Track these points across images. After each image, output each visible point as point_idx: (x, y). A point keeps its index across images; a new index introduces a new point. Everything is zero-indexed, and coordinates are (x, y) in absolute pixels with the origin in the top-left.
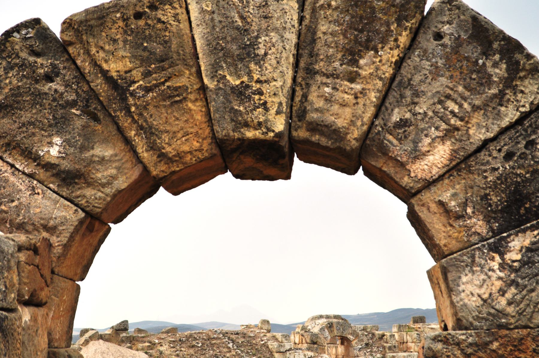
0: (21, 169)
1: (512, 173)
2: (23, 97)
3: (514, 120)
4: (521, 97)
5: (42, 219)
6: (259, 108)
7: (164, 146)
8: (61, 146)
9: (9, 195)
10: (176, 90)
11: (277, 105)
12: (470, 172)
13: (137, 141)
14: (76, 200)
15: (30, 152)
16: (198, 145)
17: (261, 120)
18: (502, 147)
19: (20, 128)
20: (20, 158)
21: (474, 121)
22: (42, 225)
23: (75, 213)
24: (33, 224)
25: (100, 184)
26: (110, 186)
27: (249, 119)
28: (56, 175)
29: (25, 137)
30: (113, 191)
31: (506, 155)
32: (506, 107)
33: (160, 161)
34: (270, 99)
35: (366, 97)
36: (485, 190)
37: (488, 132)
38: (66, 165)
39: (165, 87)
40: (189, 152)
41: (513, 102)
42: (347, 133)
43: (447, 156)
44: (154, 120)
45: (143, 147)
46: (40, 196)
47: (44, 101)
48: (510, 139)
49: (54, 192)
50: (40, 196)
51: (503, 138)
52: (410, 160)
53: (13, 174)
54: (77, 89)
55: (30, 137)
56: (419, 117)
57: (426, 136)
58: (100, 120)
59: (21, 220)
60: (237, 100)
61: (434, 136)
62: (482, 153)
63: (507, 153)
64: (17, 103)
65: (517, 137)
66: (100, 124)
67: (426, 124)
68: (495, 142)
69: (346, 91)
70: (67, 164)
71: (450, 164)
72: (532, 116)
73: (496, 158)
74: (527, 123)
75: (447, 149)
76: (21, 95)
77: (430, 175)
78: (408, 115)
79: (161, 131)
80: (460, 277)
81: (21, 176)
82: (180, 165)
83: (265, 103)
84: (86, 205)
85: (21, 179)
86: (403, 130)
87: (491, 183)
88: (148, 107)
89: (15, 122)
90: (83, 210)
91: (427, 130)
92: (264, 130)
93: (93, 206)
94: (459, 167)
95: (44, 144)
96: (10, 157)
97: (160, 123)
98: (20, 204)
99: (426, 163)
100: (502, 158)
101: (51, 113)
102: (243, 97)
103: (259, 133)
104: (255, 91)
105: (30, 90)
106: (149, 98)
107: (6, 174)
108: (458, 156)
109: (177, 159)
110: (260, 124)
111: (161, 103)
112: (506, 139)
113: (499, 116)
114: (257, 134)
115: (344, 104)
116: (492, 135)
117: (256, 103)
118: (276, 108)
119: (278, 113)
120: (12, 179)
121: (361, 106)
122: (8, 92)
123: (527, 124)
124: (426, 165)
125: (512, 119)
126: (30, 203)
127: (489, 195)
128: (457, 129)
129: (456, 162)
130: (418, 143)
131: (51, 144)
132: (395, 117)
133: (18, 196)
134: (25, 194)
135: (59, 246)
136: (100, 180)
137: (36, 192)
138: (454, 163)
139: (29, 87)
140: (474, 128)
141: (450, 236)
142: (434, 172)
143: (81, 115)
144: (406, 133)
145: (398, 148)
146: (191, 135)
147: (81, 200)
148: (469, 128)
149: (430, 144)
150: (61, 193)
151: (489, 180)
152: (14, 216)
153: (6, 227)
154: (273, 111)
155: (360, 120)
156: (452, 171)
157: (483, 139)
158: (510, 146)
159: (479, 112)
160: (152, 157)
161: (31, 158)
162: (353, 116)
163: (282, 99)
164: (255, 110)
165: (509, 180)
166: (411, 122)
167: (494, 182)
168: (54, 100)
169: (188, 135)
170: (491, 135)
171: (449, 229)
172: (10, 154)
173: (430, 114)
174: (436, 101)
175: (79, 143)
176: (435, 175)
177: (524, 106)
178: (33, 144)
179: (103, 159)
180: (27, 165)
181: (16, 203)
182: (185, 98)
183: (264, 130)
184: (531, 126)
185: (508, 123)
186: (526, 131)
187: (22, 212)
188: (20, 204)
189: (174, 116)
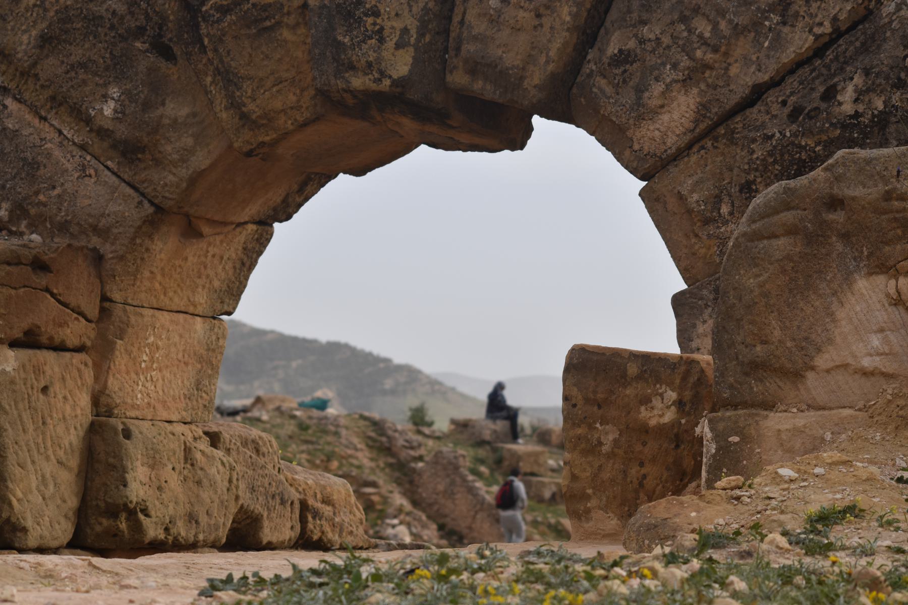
0: (69, 136)
1: (793, 143)
2: (72, 24)
3: (804, 49)
4: (819, 8)
5: (90, 215)
6: (372, 38)
7: (245, 101)
8: (119, 100)
9: (50, 178)
10: (265, 10)
11: (398, 33)
12: (732, 142)
13: (214, 92)
14: (141, 187)
15: (79, 111)
16: (294, 98)
17: (371, 59)
18: (789, 97)
19: (67, 72)
20: (68, 119)
21: (738, 52)
22: (91, 226)
23: (137, 207)
24: (78, 224)
25: (170, 161)
26: (185, 165)
27: (354, 56)
28: (114, 146)
29: (72, 86)
30: (190, 172)
31: (792, 111)
32: (793, 26)
33: (243, 126)
34: (389, 24)
35: (555, 15)
36: (748, 174)
37: (759, 71)
38: (122, 131)
39: (250, 5)
40: (283, 110)
41: (804, 17)
42: (522, 78)
43: (690, 115)
44: (232, 60)
45: (221, 103)
46: (93, 180)
47: (99, 29)
48: (801, 83)
49: (114, 173)
50: (93, 180)
51: (790, 81)
52: (631, 121)
53: (61, 145)
54: (147, 9)
55: (80, 86)
56: (649, 47)
57: (657, 79)
58: (175, 59)
59: (62, 217)
60: (343, 26)
61: (668, 80)
62: (755, 110)
63: (794, 107)
64: (66, 32)
65: (813, 79)
66: (175, 64)
67: (659, 58)
68: (778, 89)
69: (522, 4)
70: (124, 129)
71: (695, 128)
72: (841, 42)
73: (775, 116)
74: (830, 55)
75: (692, 101)
76: (70, 19)
77: (663, 148)
78: (632, 44)
79: (241, 77)
80: (694, 326)
81: (70, 148)
82: (270, 133)
83: (382, 29)
84: (153, 194)
85: (71, 152)
86: (622, 69)
87: (758, 162)
88: (224, 39)
89: (63, 62)
90: (152, 203)
91: (658, 69)
92: (376, 75)
93: (163, 197)
94: (715, 134)
95: (98, 98)
96: (56, 119)
97: (240, 64)
98: (65, 191)
99: (658, 126)
100: (785, 118)
101: (108, 47)
102: (352, 21)
103: (370, 80)
104: (368, 10)
105: (82, 12)
106: (226, 24)
107: (49, 145)
108: (708, 115)
109: (264, 122)
110: (370, 65)
111: (243, 32)
112: (795, 83)
113: (778, 42)
114: (367, 81)
115: (518, 27)
116: (766, 77)
117: (367, 30)
118: (397, 38)
119: (398, 46)
120: (57, 153)
121: (546, 28)
122: (53, 17)
123: (831, 57)
124: (658, 129)
125: (801, 48)
126: (77, 192)
127: (754, 182)
128: (707, 67)
129: (705, 124)
130: (643, 92)
131: (105, 97)
132: (612, 49)
133: (62, 181)
134: (72, 175)
135: (113, 258)
136: (170, 155)
137: (87, 173)
138: (702, 126)
139: (81, 8)
140: (737, 65)
141: (694, 254)
142: (669, 142)
143: (147, 51)
144: (626, 75)
145: (611, 100)
146: (285, 84)
147: (148, 187)
148: (729, 64)
149: (663, 93)
150: (122, 175)
151: (755, 156)
152: (54, 212)
153: (47, 227)
154: (390, 44)
155: (544, 55)
156: (704, 141)
157: (750, 84)
158: (799, 95)
159: (746, 36)
160: (233, 118)
161: (82, 120)
162: (533, 48)
163: (408, 22)
164: (364, 41)
165: (786, 156)
166: (636, 56)
167: (763, 160)
168: (112, 27)
169: (281, 82)
170: (765, 77)
171: (693, 240)
172: (56, 113)
173: (666, 40)
174: (676, 17)
175: (142, 96)
176: (670, 148)
177: (821, 24)
178: (83, 98)
179: (175, 121)
180: (78, 131)
181: (58, 191)
182: (279, 24)
183: (376, 75)
184: (836, 58)
185: (793, 56)
186: (828, 67)
187: (65, 204)
188: (65, 191)
189: (262, 53)
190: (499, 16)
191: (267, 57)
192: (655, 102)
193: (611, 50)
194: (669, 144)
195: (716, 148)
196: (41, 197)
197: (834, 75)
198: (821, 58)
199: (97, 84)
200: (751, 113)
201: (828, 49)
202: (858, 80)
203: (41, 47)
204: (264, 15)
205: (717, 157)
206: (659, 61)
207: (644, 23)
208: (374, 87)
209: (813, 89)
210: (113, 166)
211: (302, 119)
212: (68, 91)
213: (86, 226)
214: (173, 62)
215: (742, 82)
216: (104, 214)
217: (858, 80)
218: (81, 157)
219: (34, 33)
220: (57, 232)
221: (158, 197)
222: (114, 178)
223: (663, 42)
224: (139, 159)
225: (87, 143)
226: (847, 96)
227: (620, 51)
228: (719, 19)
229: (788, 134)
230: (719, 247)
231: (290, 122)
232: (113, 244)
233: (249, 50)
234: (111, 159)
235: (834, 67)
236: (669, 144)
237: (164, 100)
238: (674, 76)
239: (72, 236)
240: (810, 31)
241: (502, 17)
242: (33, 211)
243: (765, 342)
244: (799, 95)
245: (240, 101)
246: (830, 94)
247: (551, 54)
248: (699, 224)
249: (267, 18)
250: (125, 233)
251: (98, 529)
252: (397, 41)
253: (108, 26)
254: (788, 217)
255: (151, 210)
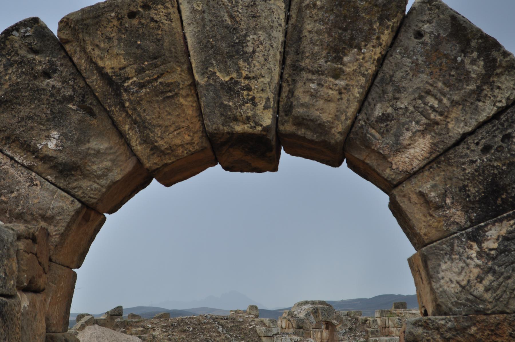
0: (20, 161)
1: (490, 165)
4: (498, 93)
5: (40, 209)
8: (58, 139)
9: (9, 186)
10: (168, 86)
11: (264, 100)
13: (131, 134)
14: (73, 192)
17: (249, 115)
18: (480, 140)
20: (19, 151)
21: (453, 115)
22: (40, 215)
23: (71, 204)
25: (95, 176)
26: (105, 178)
28: (54, 167)
29: (23, 131)
30: (108, 182)
32: (484, 102)
33: (153, 154)
34: (258, 95)
35: (350, 93)
37: (466, 126)
38: (63, 158)
39: (158, 83)
40: (181, 145)
41: (490, 98)
43: (427, 149)
44: (147, 115)
45: (137, 140)
47: (42, 96)
49: (52, 183)
50: (39, 188)
51: (481, 131)
53: (12, 166)
55: (29, 130)
57: (407, 130)
58: (95, 115)
59: (20, 210)
60: (226, 96)
61: (414, 130)
62: (461, 146)
63: (485, 146)
64: (17, 98)
65: (494, 131)
68: (473, 136)
70: (64, 157)
72: (509, 111)
73: (474, 151)
74: (503, 118)
75: (427, 142)
76: (20, 90)
77: (411, 167)
78: (390, 110)
80: (439, 265)
82: (172, 158)
84: (82, 195)
86: (385, 124)
87: (469, 175)
88: (141, 102)
89: (15, 116)
90: (79, 201)
92: (253, 124)
94: (438, 160)
95: (42, 137)
97: (153, 118)
98: (20, 194)
99: (407, 156)
100: (480, 151)
102: (232, 93)
103: (248, 127)
104: (244, 87)
105: (29, 86)
106: (143, 94)
108: (438, 149)
109: (169, 152)
110: (248, 118)
111: (154, 99)
112: (484, 133)
113: (476, 111)
114: (246, 128)
115: (329, 99)
116: (470, 129)
117: (244, 99)
118: (264, 103)
119: (266, 108)
121: (345, 101)
122: (8, 88)
124: (407, 157)
125: (489, 114)
126: (28, 194)
127: (467, 186)
128: (437, 123)
130: (399, 137)
131: (48, 138)
132: (378, 112)
133: (17, 188)
134: (24, 185)
135: (56, 235)
136: (96, 172)
137: (35, 183)
138: (434, 156)
139: (28, 84)
140: (453, 122)
141: (430, 226)
142: (415, 164)
143: (77, 110)
145: (380, 141)
146: (182, 129)
147: (77, 191)
150: (58, 184)
152: (14, 207)
154: (261, 106)
157: (461, 133)
158: (488, 139)
159: (457, 107)
160: (145, 150)
161: (29, 151)
162: (337, 111)
163: (269, 94)
164: (243, 105)
166: (393, 117)
167: (473, 174)
168: (52, 95)
169: (179, 129)
170: (469, 129)
171: (429, 218)
172: (10, 147)
173: (411, 108)
174: (417, 96)
176: (415, 168)
177: (500, 101)
180: (26, 158)
181: (15, 194)
183: (253, 124)
184: (507, 120)
185: (485, 118)
186: (502, 125)
187: (21, 202)
188: (20, 194)
189: (166, 111)
190: (317, 93)
191: (169, 114)
192: (406, 142)
193: (377, 114)
194: (414, 165)
195: (440, 167)
197: (507, 129)
198: (498, 120)
199: (41, 129)
200: (459, 149)
201: (501, 115)
204: (168, 89)
205: (441, 172)
206: (408, 120)
207: (397, 99)
209: (495, 136)
210: (51, 179)
211: (194, 150)
212: (21, 133)
213: (37, 215)
214: (95, 117)
215: (457, 132)
216: (50, 208)
218: (28, 174)
220: (14, 220)
221: (85, 197)
222: (53, 186)
223: (409, 110)
224: (72, 175)
225: (34, 165)
227: (383, 114)
228: (442, 97)
229: (485, 160)
230: (445, 222)
231: (186, 152)
232: (55, 226)
233: (158, 109)
234: (50, 175)
235: (506, 124)
236: (414, 165)
237: (89, 139)
238: (418, 128)
240: (494, 105)
241: (319, 93)
244: (488, 139)
245: (153, 139)
247: (349, 114)
248: (433, 209)
249: (170, 91)
250: (64, 219)
252: (264, 105)
253: (49, 94)
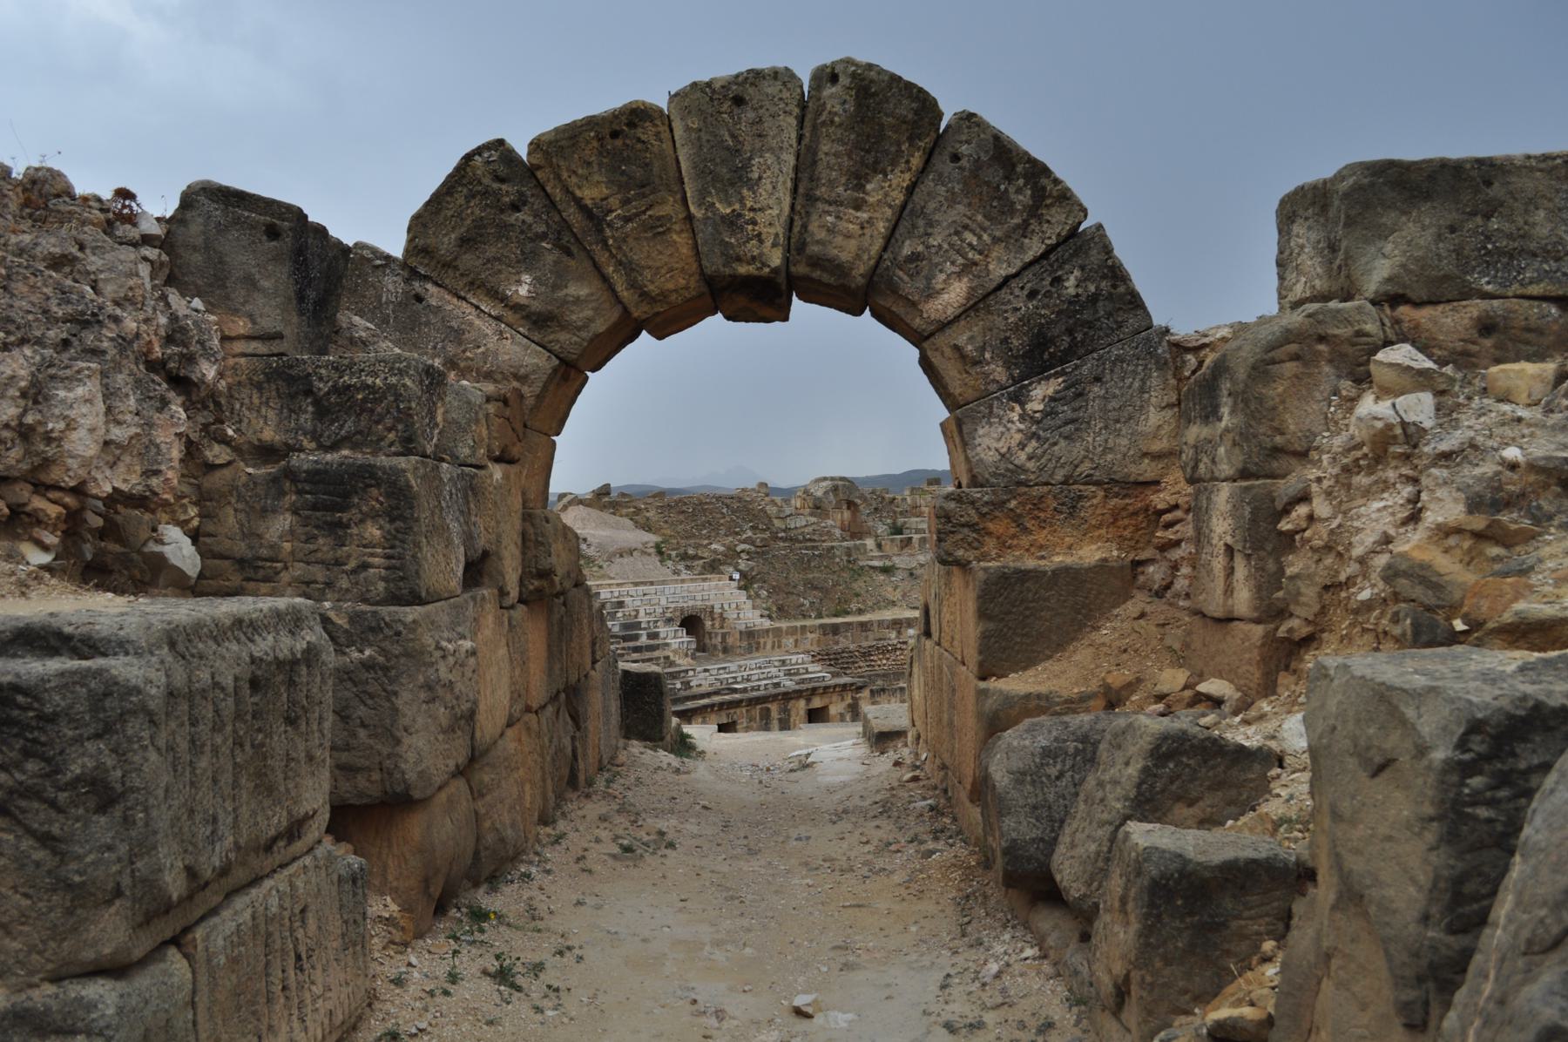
12: (989, 312)
14: (549, 346)
15: (497, 292)
16: (684, 282)
21: (994, 254)
38: (536, 306)
53: (478, 317)
56: (933, 250)
57: (941, 271)
62: (1003, 291)
74: (1053, 257)
75: (964, 286)
78: (920, 248)
110: (754, 258)
120: (477, 322)
121: (867, 237)
128: (975, 264)
131: (519, 282)
138: (971, 302)
142: (949, 312)
154: (768, 244)
168: (522, 232)
170: (1013, 271)
173: (946, 246)
182: (669, 229)
186: (1052, 266)
188: (487, 350)
192: (939, 286)
196: (468, 354)
202: (1077, 273)
203: (461, 246)
204: (658, 223)
207: (929, 235)
208: (756, 273)
217: (1077, 273)
219: (453, 236)
226: (1071, 283)
239: (496, 381)
242: (462, 365)
243: (1282, 434)
246: (1057, 281)
251: (531, 587)
254: (1293, 348)
255: (557, 362)
